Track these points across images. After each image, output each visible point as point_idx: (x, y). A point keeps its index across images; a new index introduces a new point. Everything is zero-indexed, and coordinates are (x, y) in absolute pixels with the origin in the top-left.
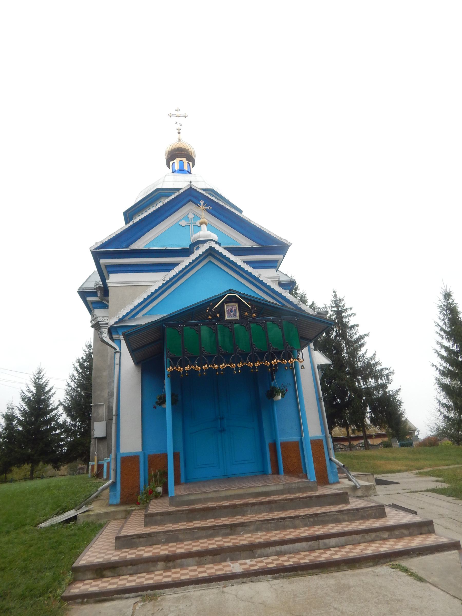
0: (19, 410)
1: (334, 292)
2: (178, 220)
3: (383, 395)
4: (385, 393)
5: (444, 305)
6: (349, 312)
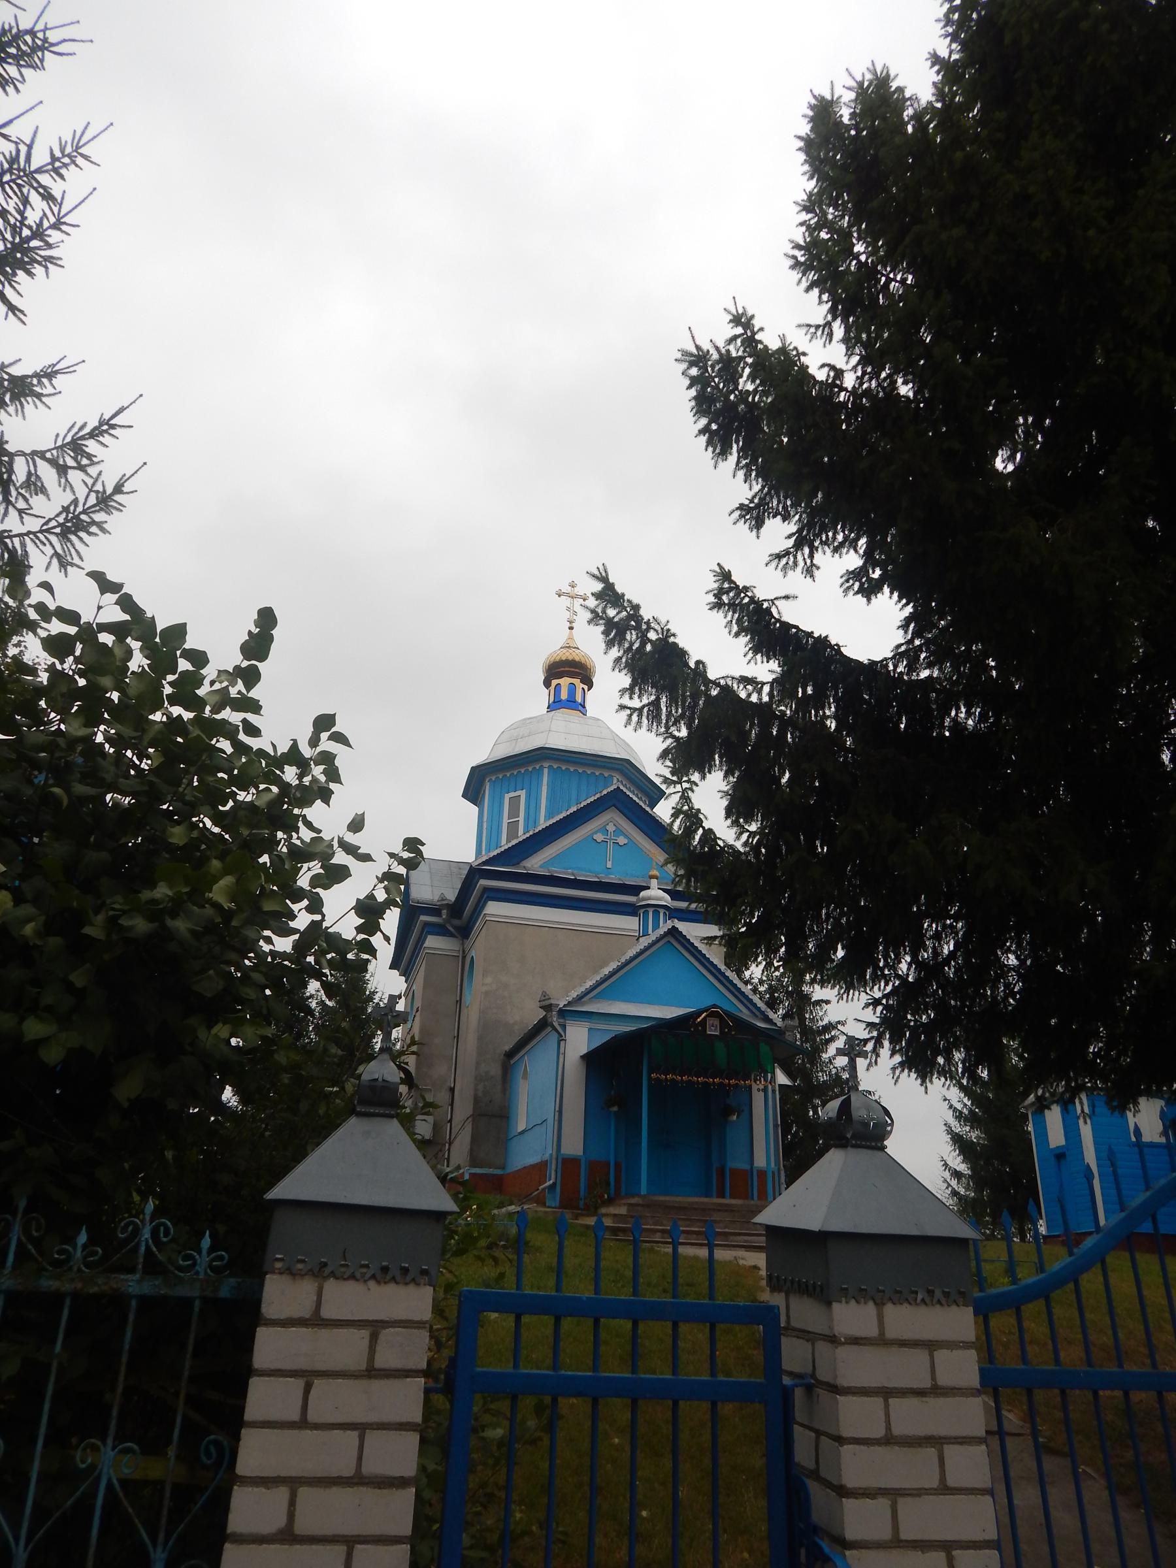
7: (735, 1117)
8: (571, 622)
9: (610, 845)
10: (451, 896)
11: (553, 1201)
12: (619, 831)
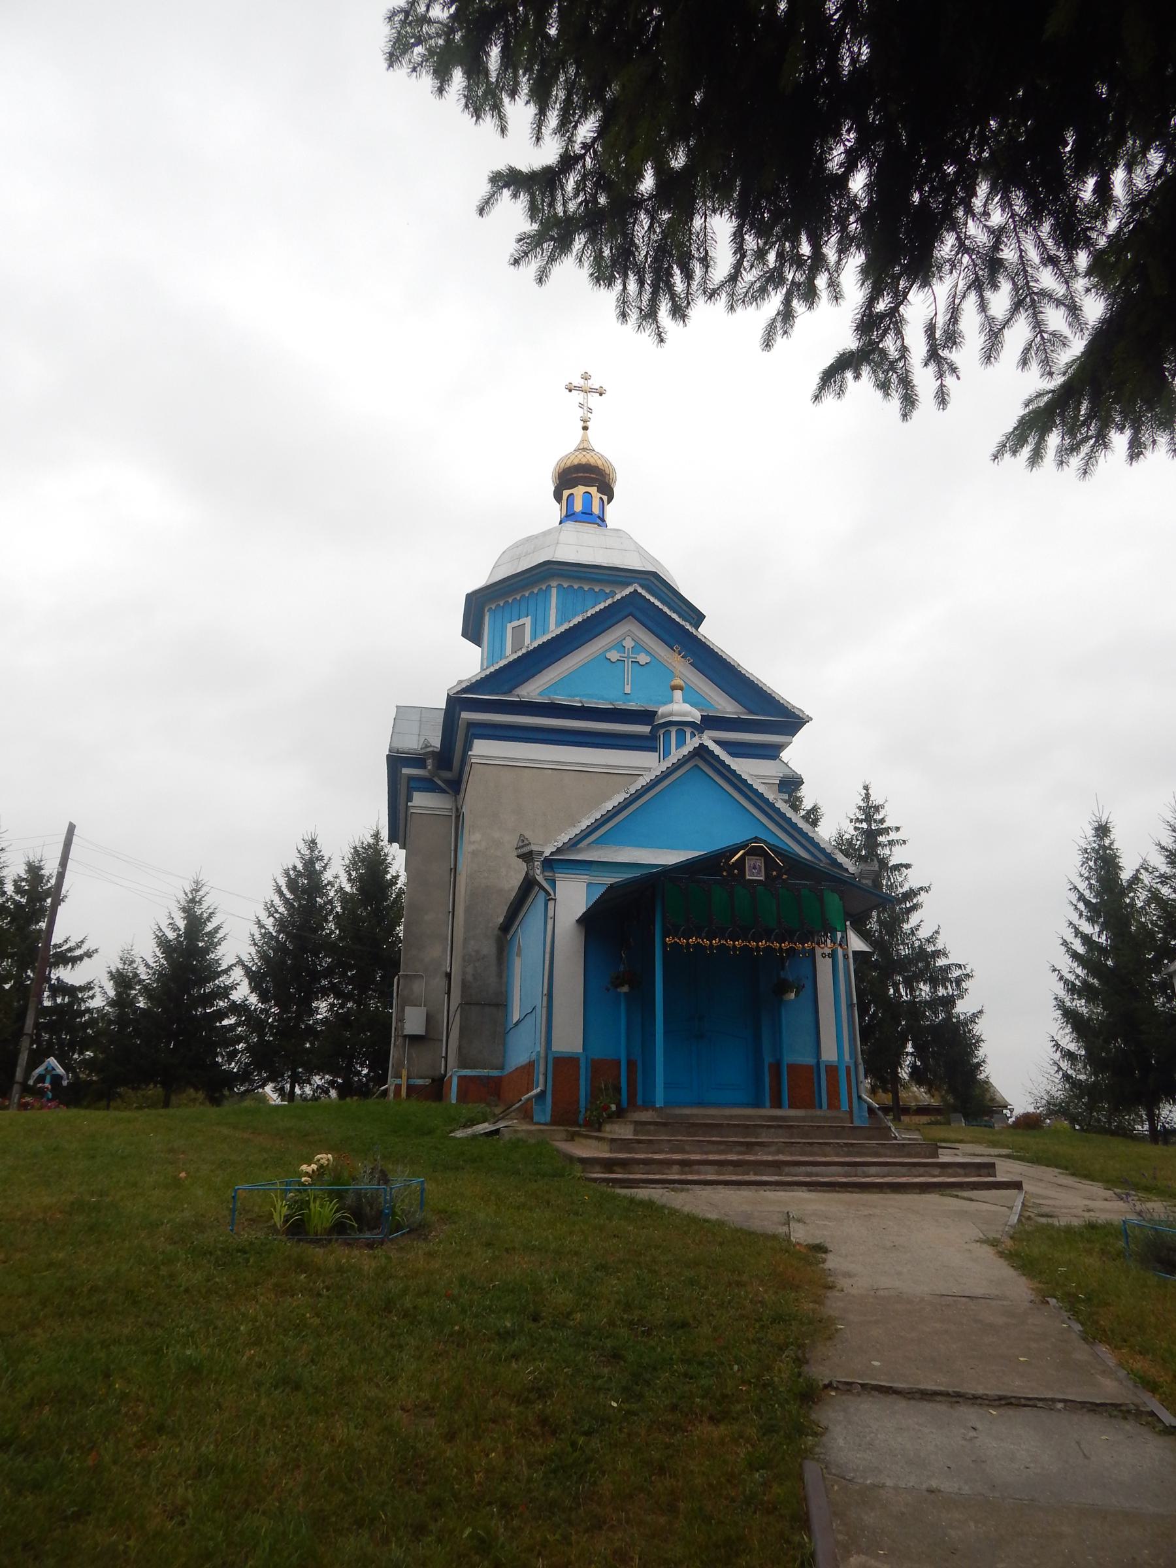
0: (147, 965)
1: (866, 788)
3: (944, 1019)
4: (950, 1015)
6: (893, 836)
7: (793, 996)
8: (585, 421)
9: (628, 665)
10: (436, 742)
11: (543, 1114)
12: (639, 647)
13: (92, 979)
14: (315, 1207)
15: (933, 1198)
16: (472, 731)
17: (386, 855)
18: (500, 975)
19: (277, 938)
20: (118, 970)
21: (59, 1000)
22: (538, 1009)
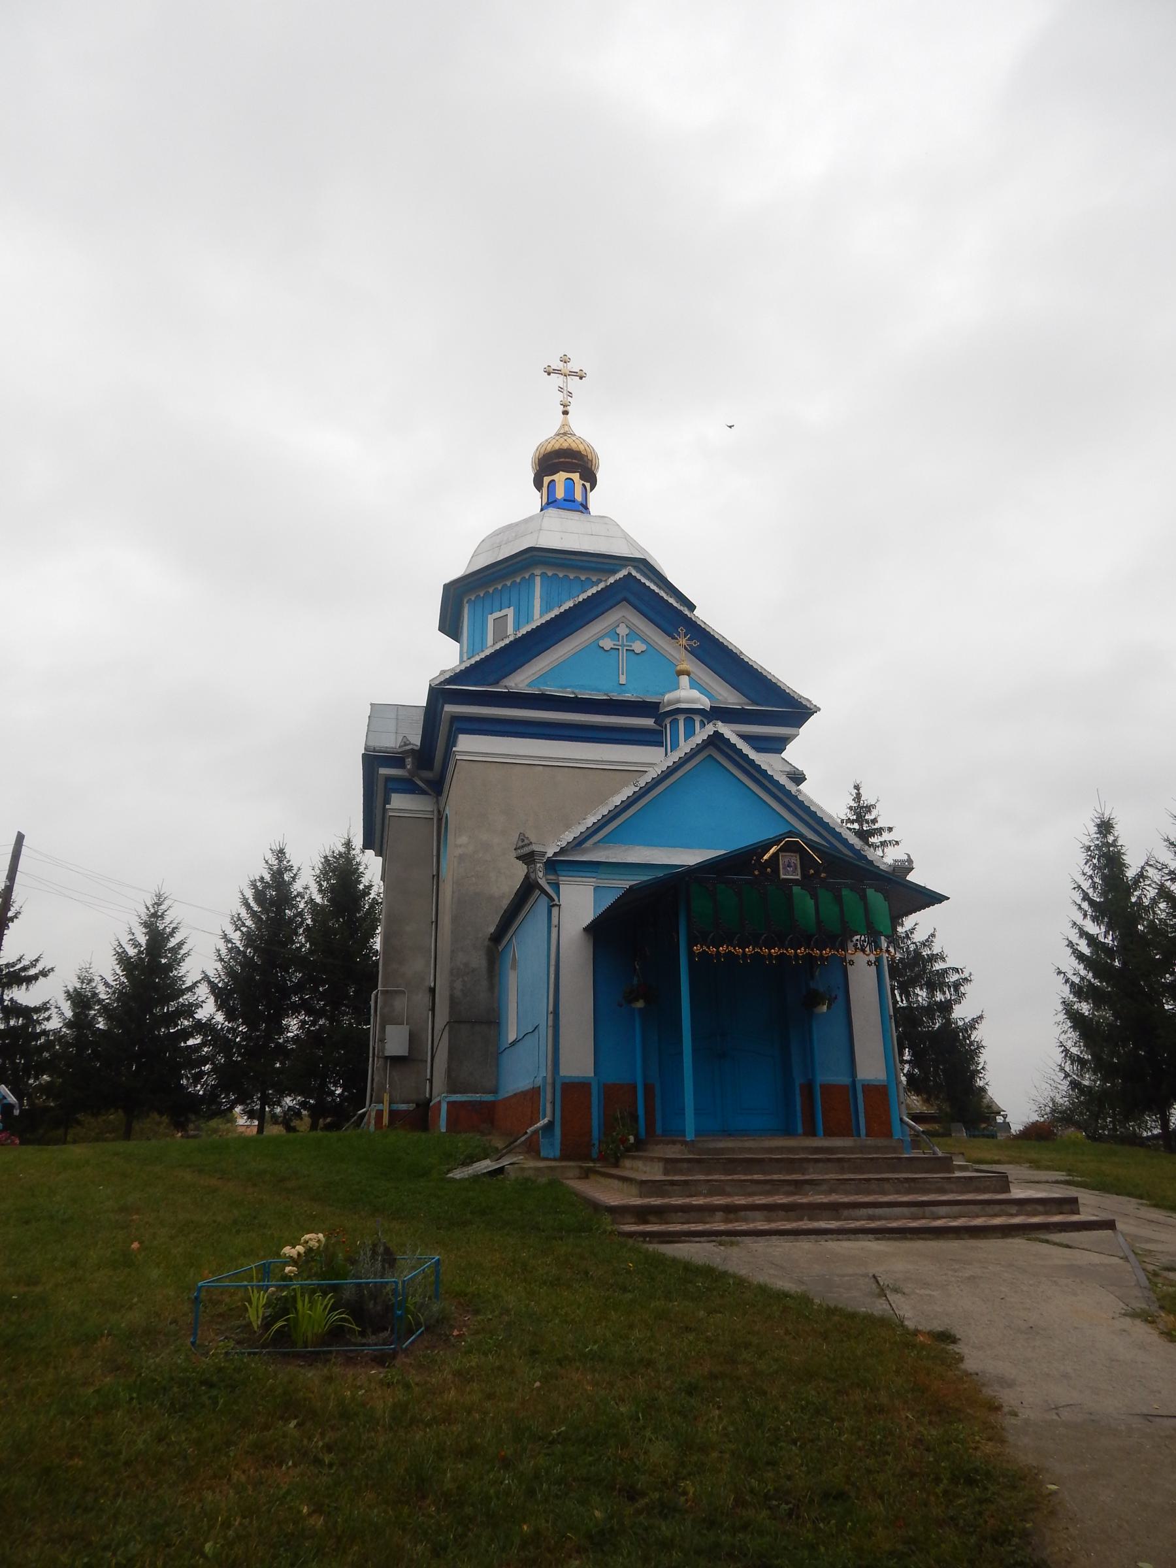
0: (106, 984)
1: (857, 787)
2: (599, 635)
4: (948, 1022)
5: (1097, 846)
6: (886, 836)
7: (825, 1008)
9: (623, 654)
10: (416, 740)
11: (552, 1148)
12: (634, 634)
13: (49, 998)
14: (302, 1306)
15: (1018, 1244)
16: (456, 725)
17: (359, 864)
18: (492, 987)
19: (244, 952)
20: (75, 989)
21: (12, 1023)
22: (542, 1028)
